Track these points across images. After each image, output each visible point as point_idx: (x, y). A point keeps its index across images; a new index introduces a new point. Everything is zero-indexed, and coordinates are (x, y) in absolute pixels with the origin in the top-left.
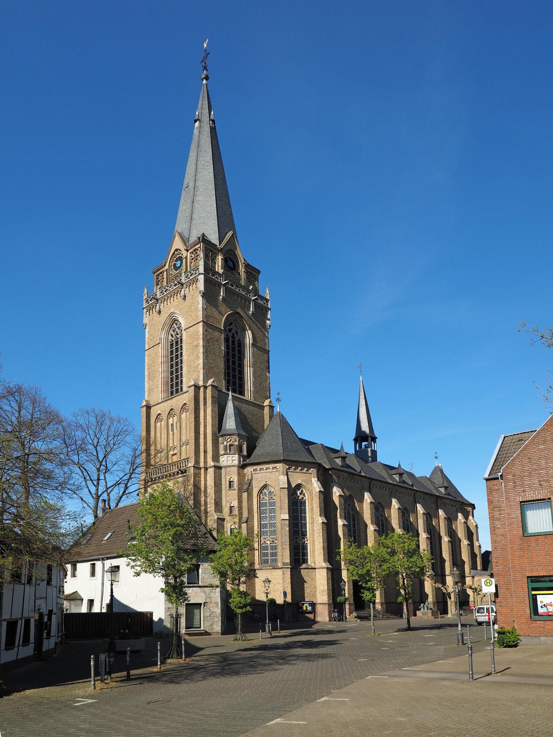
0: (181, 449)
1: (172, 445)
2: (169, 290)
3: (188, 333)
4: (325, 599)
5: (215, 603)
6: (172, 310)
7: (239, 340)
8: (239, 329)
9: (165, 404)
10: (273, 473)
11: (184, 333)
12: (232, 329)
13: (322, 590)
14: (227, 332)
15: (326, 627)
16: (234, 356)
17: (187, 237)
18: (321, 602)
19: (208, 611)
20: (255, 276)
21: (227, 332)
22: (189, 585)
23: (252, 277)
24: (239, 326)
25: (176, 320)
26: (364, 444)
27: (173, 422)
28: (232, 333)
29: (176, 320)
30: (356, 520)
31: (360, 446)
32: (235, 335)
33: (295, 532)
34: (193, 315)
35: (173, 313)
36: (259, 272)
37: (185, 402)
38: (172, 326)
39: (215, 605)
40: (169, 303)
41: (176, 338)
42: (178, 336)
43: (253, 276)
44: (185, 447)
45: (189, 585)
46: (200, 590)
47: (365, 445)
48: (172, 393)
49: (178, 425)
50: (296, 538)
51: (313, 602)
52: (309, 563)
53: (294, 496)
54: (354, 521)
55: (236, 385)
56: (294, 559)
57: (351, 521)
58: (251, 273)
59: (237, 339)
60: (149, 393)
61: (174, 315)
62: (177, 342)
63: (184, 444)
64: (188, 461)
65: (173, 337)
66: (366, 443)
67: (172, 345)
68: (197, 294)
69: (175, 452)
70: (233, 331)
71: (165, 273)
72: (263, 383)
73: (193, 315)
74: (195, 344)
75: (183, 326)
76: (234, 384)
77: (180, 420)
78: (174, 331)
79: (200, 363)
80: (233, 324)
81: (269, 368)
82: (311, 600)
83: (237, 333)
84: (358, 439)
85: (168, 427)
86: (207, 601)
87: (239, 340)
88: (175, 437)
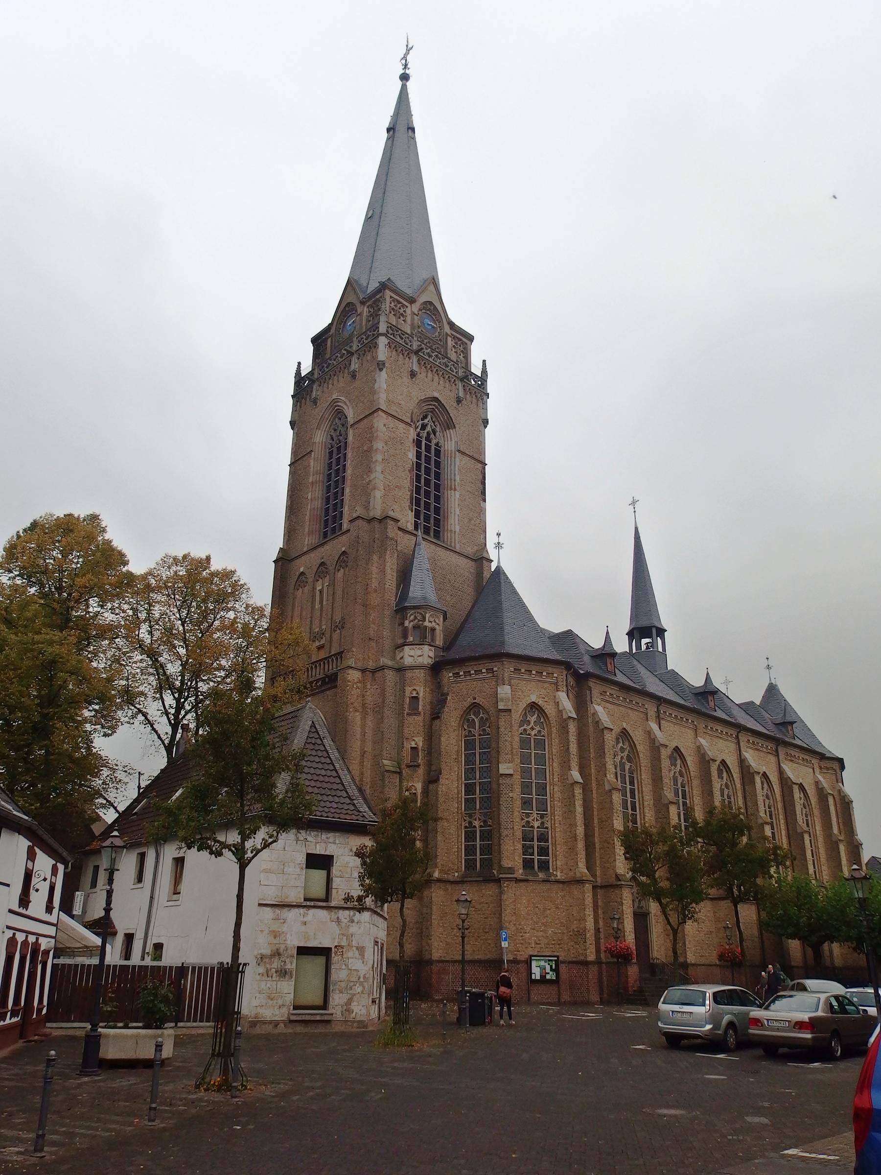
0: (333, 635)
1: (317, 629)
2: (332, 364)
3: (356, 431)
4: (581, 952)
5: (357, 948)
6: (334, 397)
7: (437, 444)
8: (438, 426)
9: (312, 555)
10: (486, 681)
11: (351, 432)
12: (427, 425)
13: (576, 930)
14: (418, 430)
15: (589, 1016)
16: (428, 471)
17: (365, 285)
18: (574, 959)
19: (344, 967)
20: (466, 344)
21: (418, 430)
22: (308, 903)
23: (460, 346)
24: (438, 421)
25: (339, 412)
26: (644, 641)
27: (323, 588)
28: (426, 431)
29: (339, 412)
30: (636, 782)
31: (639, 646)
32: (432, 436)
33: (525, 803)
34: (366, 401)
35: (335, 401)
36: (471, 338)
37: (343, 549)
38: (332, 422)
39: (357, 952)
40: (330, 386)
41: (338, 441)
42: (341, 438)
43: (462, 343)
44: (338, 631)
45: (308, 903)
46: (329, 917)
47: (647, 644)
48: (325, 535)
49: (331, 589)
50: (528, 815)
51: (558, 957)
52: (551, 871)
53: (522, 728)
54: (632, 783)
55: (429, 520)
56: (523, 861)
57: (628, 783)
58: (460, 340)
59: (434, 441)
60: (289, 536)
61: (339, 404)
62: (339, 449)
63: (337, 626)
64: (341, 657)
65: (333, 441)
66: (648, 640)
67: (331, 453)
68: (374, 367)
69: (323, 642)
70: (429, 429)
71: (329, 341)
72: (475, 519)
73: (366, 401)
74: (365, 448)
75: (351, 420)
76: (427, 518)
77: (332, 584)
78: (335, 430)
79: (371, 479)
80: (429, 417)
81: (484, 493)
82: (556, 954)
83: (434, 432)
84: (635, 632)
85: (313, 596)
86: (343, 944)
87: (437, 444)
88: (324, 615)
